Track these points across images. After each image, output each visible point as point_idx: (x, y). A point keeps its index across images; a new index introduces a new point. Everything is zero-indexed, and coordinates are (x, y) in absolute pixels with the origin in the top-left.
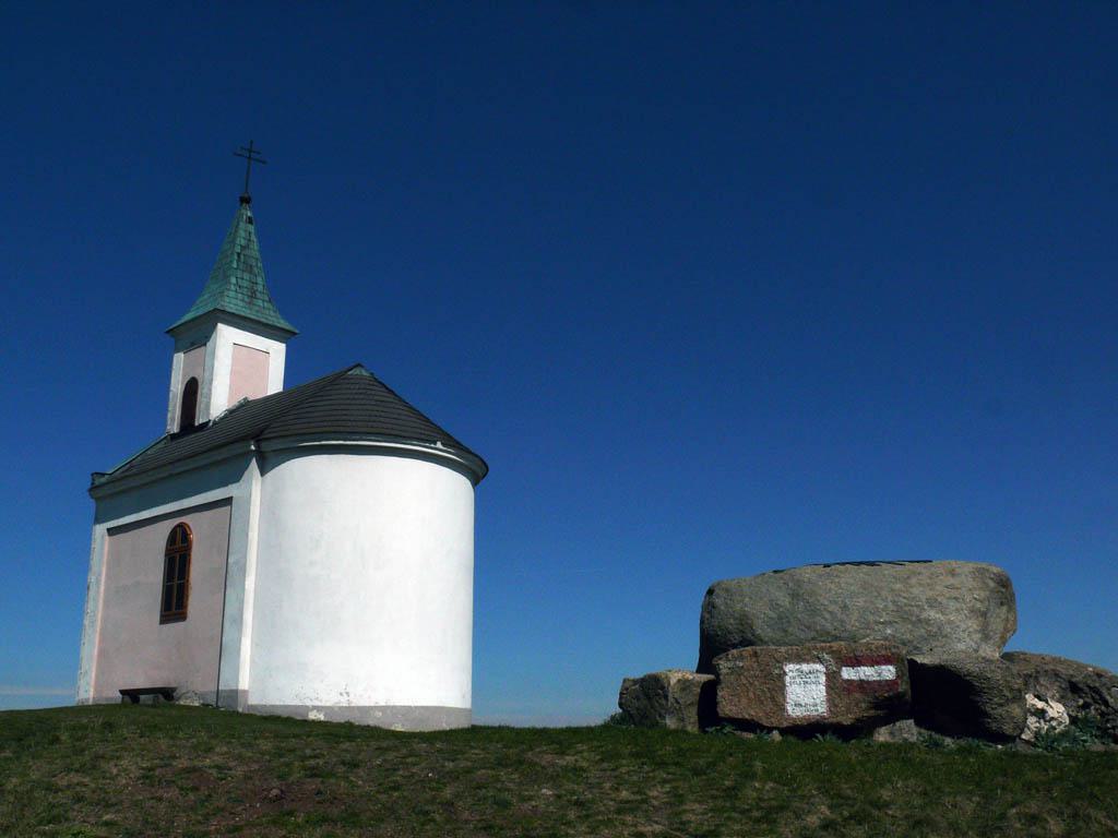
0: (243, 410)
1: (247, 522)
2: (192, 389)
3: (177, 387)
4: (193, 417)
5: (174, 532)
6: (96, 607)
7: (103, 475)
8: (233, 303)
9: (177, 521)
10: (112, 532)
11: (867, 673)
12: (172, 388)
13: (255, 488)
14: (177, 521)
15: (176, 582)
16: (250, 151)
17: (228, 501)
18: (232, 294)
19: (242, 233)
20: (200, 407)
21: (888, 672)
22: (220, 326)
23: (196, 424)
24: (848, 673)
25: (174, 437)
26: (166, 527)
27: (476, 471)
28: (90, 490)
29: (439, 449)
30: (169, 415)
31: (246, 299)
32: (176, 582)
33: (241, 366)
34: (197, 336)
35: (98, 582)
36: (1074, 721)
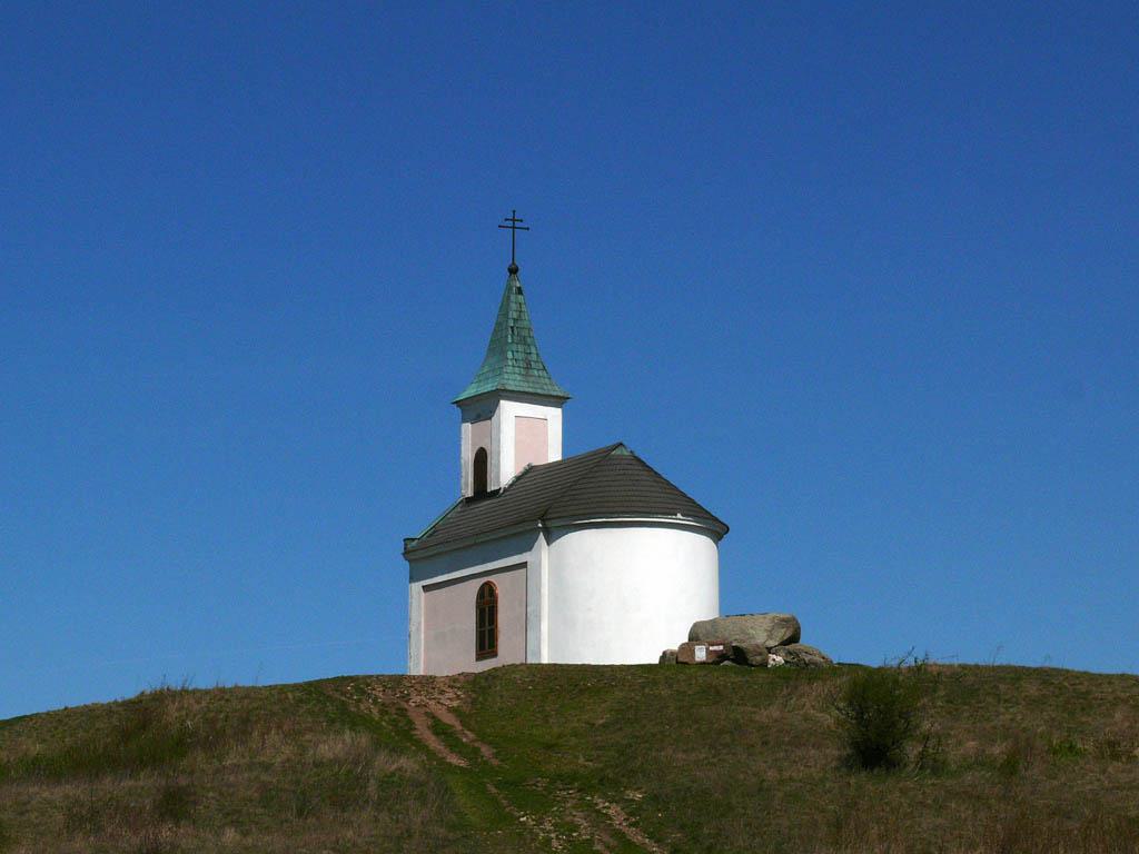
0: (530, 475)
1: (539, 605)
2: (481, 459)
3: (468, 456)
4: (485, 486)
5: (482, 588)
6: (419, 649)
7: (413, 540)
8: (513, 381)
9: (485, 579)
10: (426, 588)
11: (716, 648)
12: (463, 455)
13: (544, 556)
14: (485, 579)
15: (487, 628)
16: (514, 220)
17: (524, 565)
18: (510, 369)
19: (514, 306)
20: (491, 475)
21: (721, 648)
22: (502, 402)
23: (489, 490)
24: (711, 648)
25: (468, 500)
26: (477, 584)
27: (715, 529)
28: (404, 554)
29: (679, 518)
30: (463, 481)
31: (523, 372)
32: (487, 628)
33: (527, 437)
34: (481, 409)
35: (418, 629)
36: (786, 662)
